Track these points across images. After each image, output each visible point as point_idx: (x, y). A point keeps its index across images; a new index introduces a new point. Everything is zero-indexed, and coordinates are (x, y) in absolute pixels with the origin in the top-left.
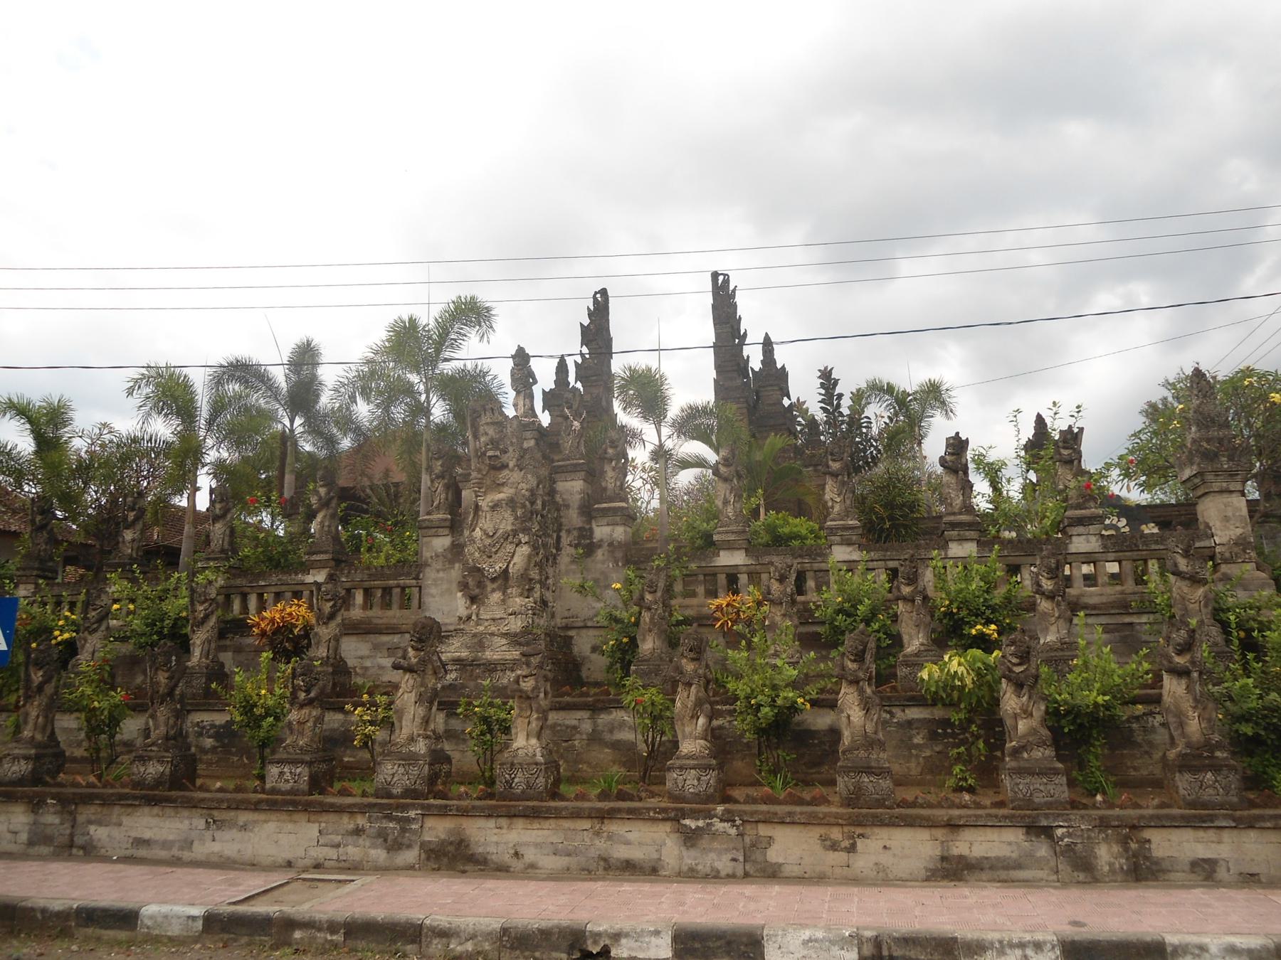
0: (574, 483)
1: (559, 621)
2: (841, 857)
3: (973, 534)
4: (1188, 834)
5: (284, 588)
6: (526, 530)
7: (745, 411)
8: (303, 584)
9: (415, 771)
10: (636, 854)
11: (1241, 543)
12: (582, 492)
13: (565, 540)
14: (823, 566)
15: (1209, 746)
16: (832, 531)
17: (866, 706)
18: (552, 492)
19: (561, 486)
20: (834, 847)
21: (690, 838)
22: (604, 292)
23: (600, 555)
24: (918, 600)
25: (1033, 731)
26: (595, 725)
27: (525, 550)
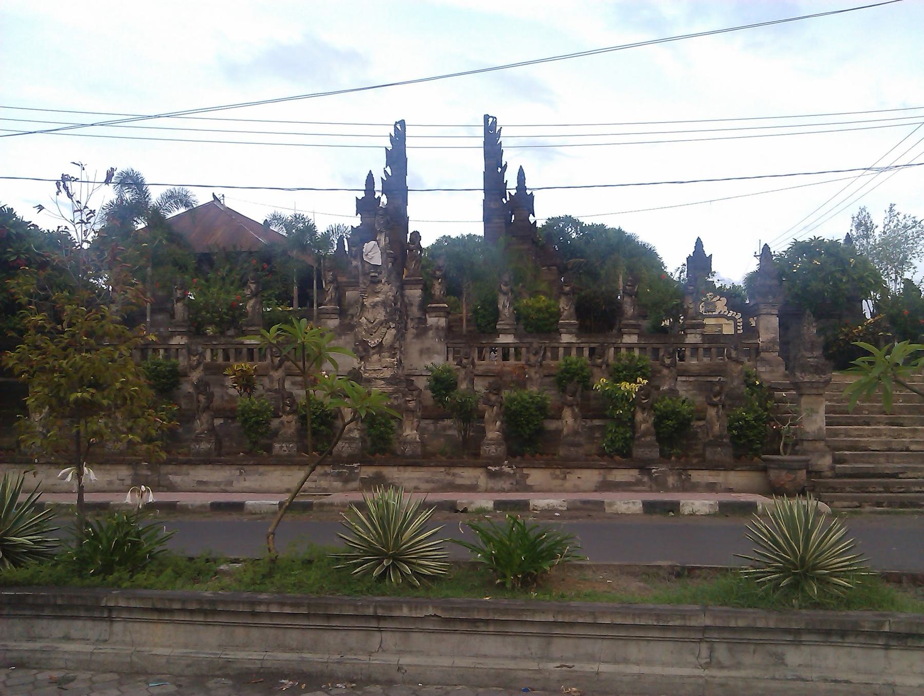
0: (415, 291)
1: (406, 372)
2: (559, 482)
3: (636, 331)
4: (706, 472)
5: (229, 346)
6: (393, 321)
7: (503, 225)
8: (242, 344)
9: (354, 445)
10: (468, 482)
11: (772, 341)
12: (420, 296)
13: (410, 324)
14: (556, 345)
15: (721, 437)
16: (563, 325)
17: (575, 418)
18: (402, 296)
19: (408, 292)
20: (557, 477)
21: (492, 475)
22: (402, 123)
23: (431, 333)
24: (604, 367)
25: (648, 429)
26: (436, 428)
27: (393, 331)
